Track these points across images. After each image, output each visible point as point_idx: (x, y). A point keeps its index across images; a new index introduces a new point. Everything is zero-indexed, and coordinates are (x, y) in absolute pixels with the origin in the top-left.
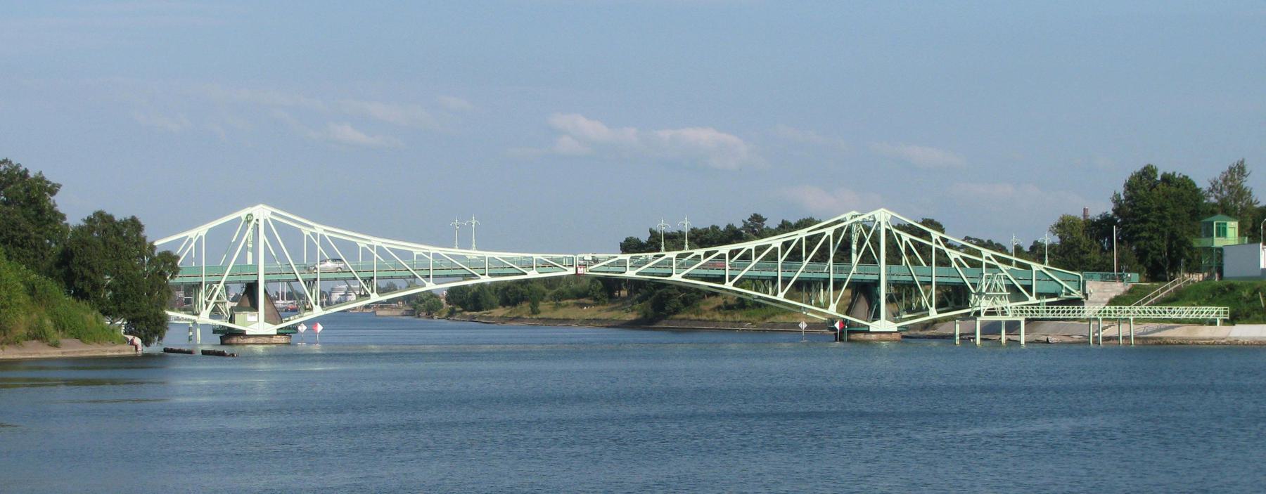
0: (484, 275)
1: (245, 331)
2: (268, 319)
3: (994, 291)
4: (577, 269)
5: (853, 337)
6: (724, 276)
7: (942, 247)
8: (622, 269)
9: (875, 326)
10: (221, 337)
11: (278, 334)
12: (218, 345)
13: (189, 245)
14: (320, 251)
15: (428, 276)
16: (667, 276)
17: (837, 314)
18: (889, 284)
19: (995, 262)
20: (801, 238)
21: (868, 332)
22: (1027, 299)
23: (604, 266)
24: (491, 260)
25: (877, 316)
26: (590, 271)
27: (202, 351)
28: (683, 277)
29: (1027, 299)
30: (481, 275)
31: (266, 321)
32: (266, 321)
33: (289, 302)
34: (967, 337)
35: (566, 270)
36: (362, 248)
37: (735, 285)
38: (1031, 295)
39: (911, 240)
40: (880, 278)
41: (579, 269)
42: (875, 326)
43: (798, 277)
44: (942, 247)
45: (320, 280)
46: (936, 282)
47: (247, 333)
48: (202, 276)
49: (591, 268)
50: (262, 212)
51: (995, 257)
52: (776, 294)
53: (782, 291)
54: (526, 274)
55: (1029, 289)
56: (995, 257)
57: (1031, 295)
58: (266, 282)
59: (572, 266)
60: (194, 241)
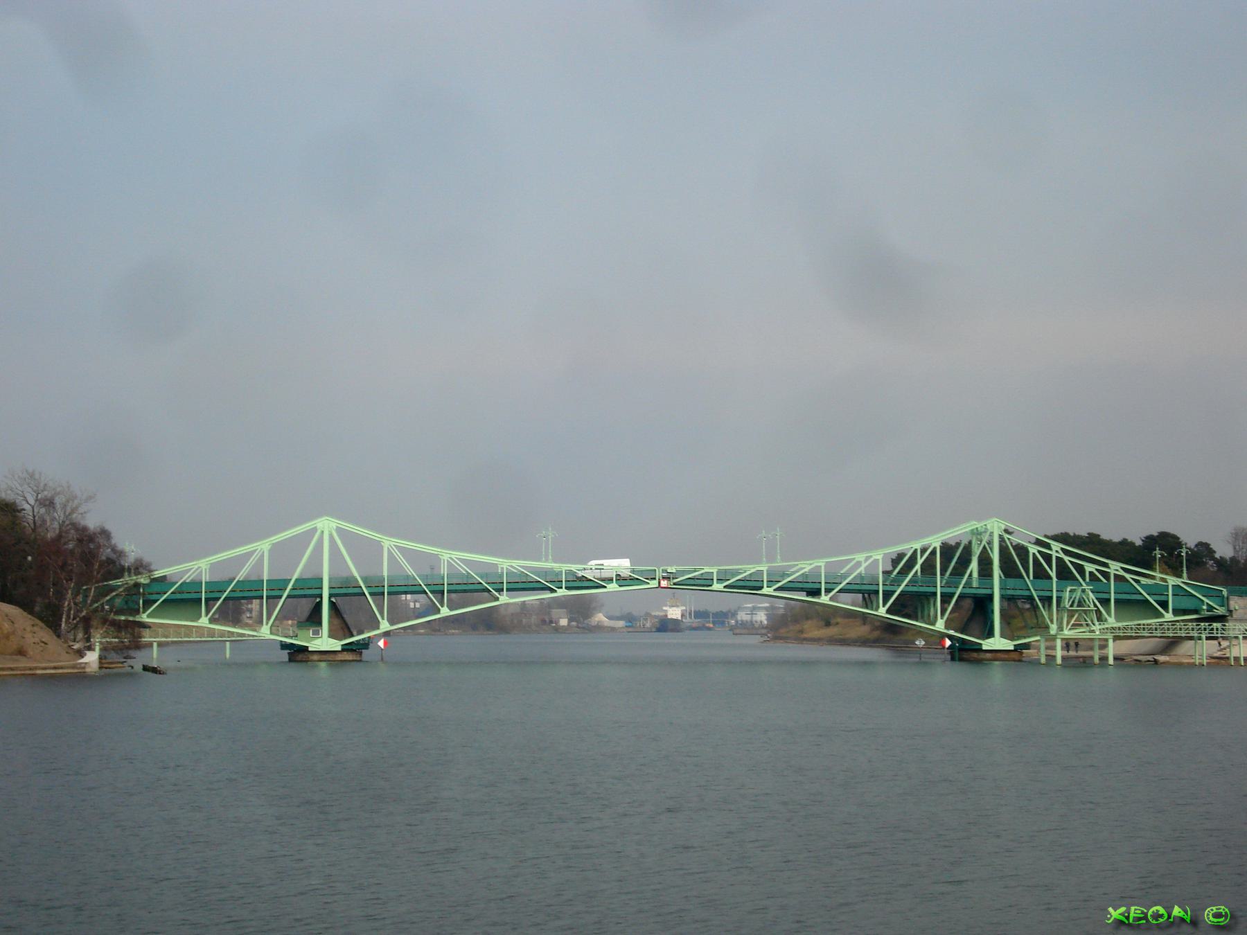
0: (561, 588)
1: (307, 647)
2: (332, 635)
3: (1078, 606)
4: (659, 583)
5: (965, 655)
6: (820, 589)
7: (1062, 555)
8: (708, 582)
9: (987, 644)
10: (289, 653)
11: (343, 650)
12: (286, 662)
13: (857, 569)
14: (1051, 570)
15: (502, 590)
16: (757, 590)
17: (945, 631)
18: (1002, 597)
19: (1122, 573)
20: (916, 550)
21: (981, 650)
22: (1163, 616)
23: (690, 578)
24: (569, 573)
25: (990, 634)
26: (674, 584)
27: (144, 666)
28: (776, 590)
29: (1163, 616)
30: (558, 588)
31: (329, 637)
32: (329, 637)
33: (697, 620)
34: (1104, 659)
35: (649, 583)
36: (1090, 572)
37: (831, 599)
38: (1168, 612)
39: (1039, 552)
40: (993, 592)
41: (662, 582)
42: (987, 644)
43: (902, 591)
44: (1062, 555)
45: (384, 593)
46: (883, 591)
47: (310, 649)
48: (263, 590)
49: (675, 581)
50: (326, 525)
51: (1122, 568)
52: (877, 609)
53: (884, 606)
54: (605, 587)
55: (1164, 605)
56: (1122, 568)
57: (1168, 612)
58: (331, 596)
59: (655, 579)
60: (920, 561)
